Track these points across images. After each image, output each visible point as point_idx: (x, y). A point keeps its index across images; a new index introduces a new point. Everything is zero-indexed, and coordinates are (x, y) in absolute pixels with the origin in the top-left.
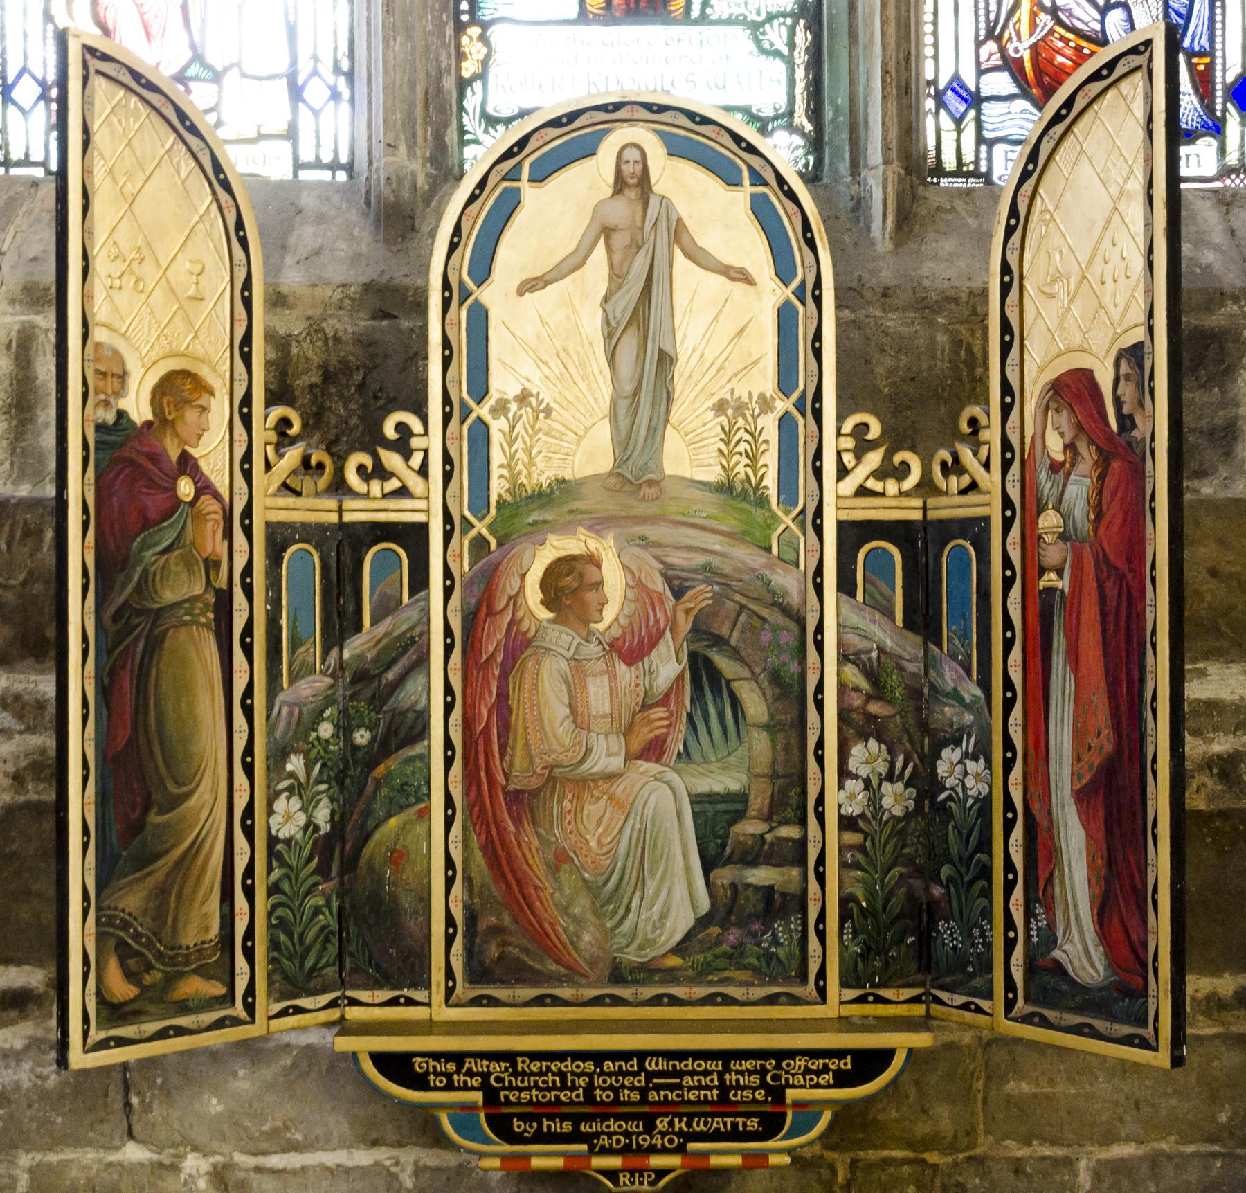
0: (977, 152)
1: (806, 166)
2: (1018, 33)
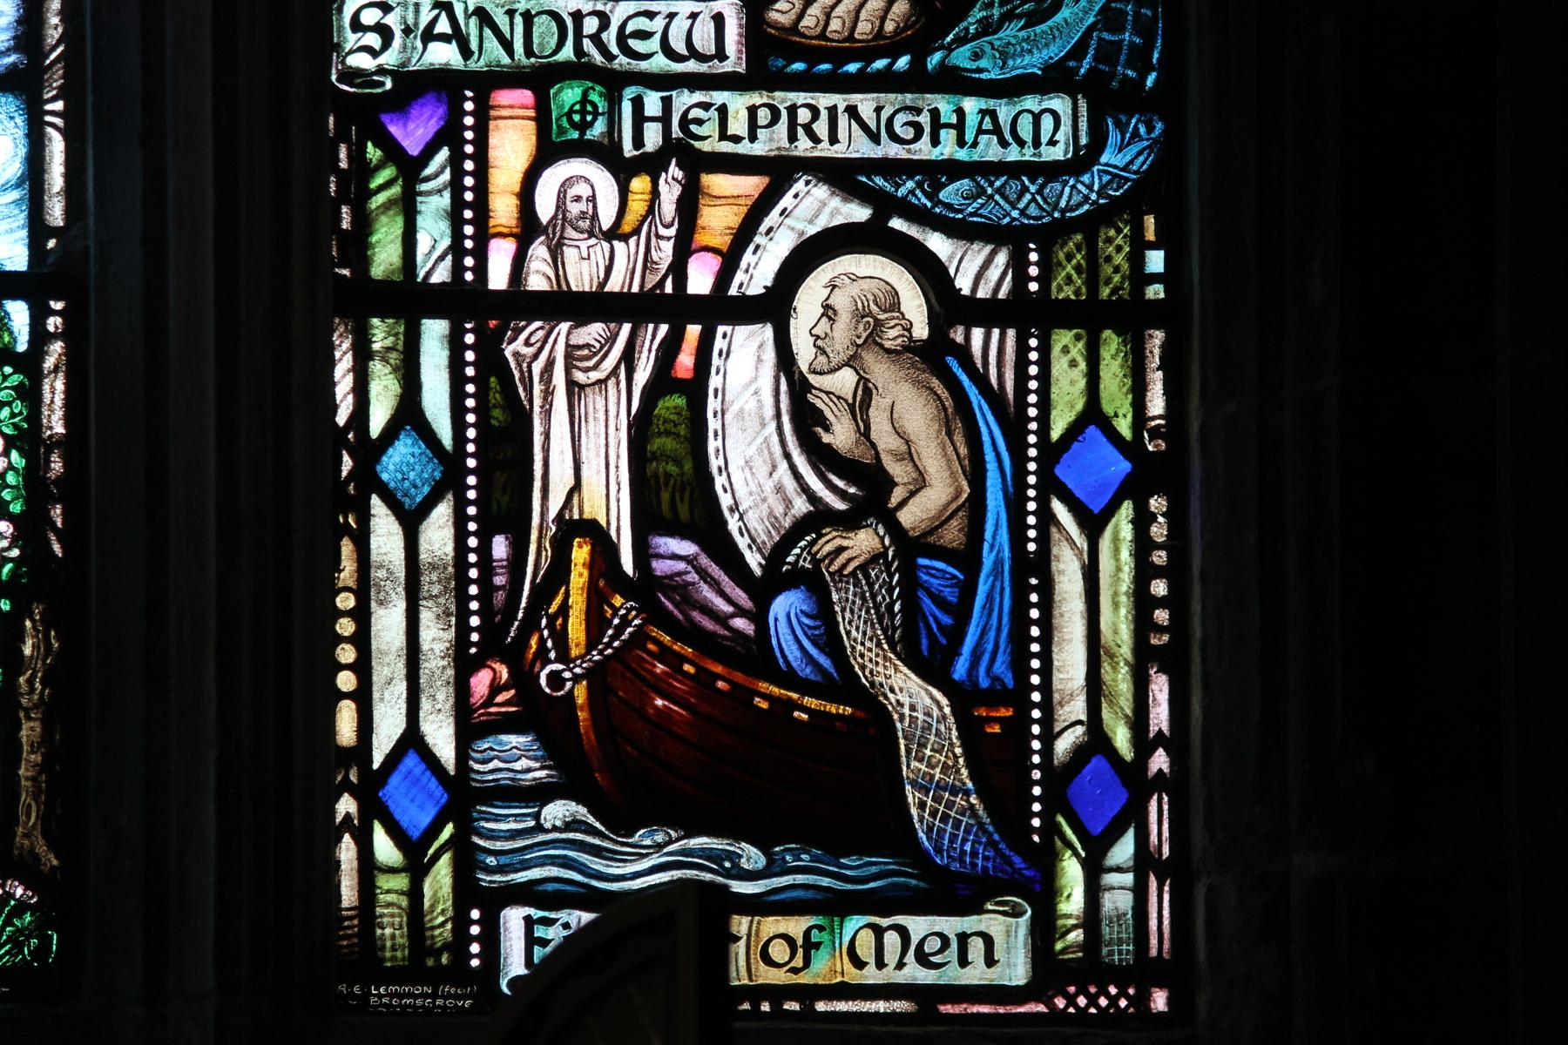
0: (460, 921)
1: (42, 950)
2: (561, 638)
